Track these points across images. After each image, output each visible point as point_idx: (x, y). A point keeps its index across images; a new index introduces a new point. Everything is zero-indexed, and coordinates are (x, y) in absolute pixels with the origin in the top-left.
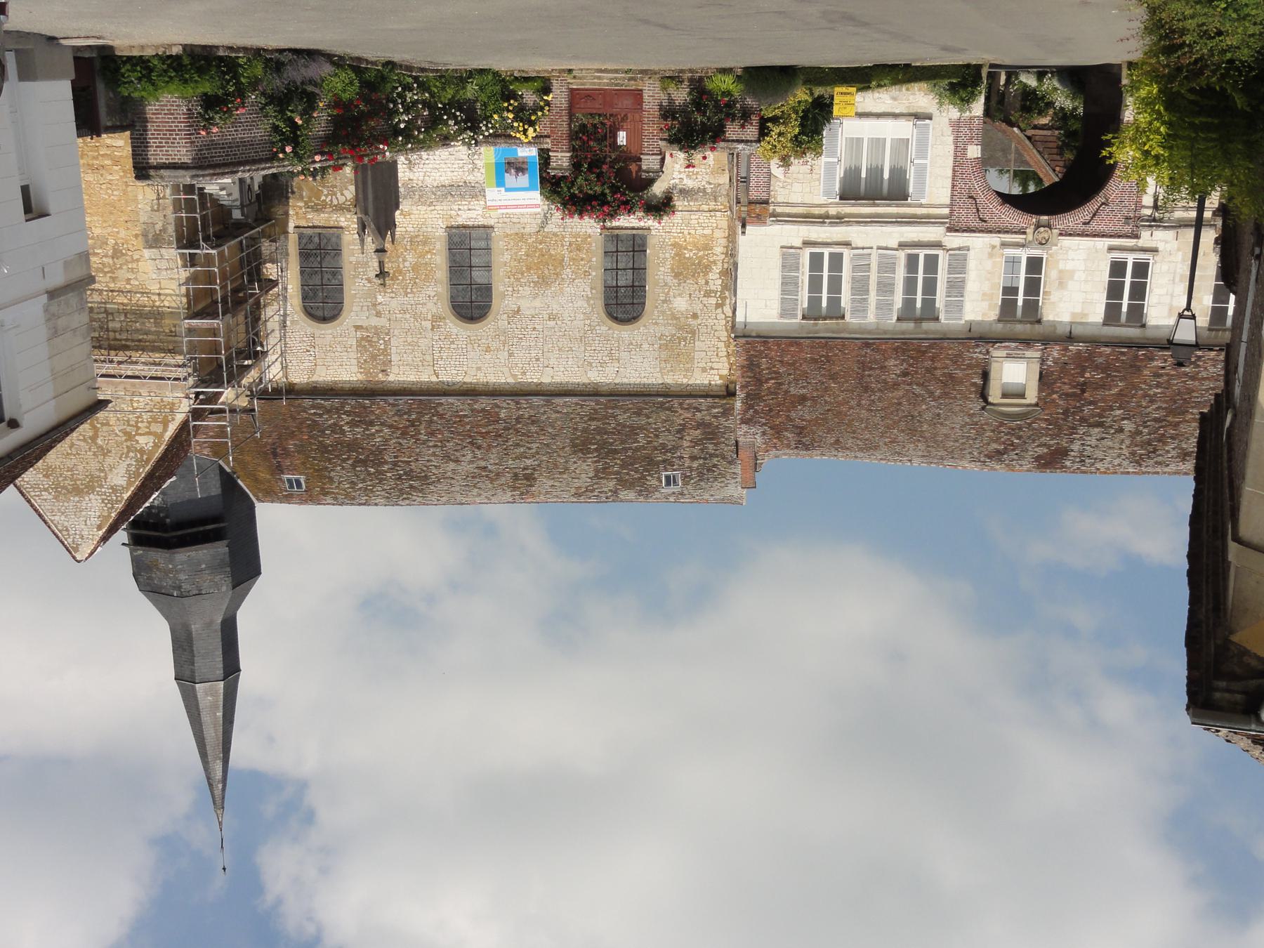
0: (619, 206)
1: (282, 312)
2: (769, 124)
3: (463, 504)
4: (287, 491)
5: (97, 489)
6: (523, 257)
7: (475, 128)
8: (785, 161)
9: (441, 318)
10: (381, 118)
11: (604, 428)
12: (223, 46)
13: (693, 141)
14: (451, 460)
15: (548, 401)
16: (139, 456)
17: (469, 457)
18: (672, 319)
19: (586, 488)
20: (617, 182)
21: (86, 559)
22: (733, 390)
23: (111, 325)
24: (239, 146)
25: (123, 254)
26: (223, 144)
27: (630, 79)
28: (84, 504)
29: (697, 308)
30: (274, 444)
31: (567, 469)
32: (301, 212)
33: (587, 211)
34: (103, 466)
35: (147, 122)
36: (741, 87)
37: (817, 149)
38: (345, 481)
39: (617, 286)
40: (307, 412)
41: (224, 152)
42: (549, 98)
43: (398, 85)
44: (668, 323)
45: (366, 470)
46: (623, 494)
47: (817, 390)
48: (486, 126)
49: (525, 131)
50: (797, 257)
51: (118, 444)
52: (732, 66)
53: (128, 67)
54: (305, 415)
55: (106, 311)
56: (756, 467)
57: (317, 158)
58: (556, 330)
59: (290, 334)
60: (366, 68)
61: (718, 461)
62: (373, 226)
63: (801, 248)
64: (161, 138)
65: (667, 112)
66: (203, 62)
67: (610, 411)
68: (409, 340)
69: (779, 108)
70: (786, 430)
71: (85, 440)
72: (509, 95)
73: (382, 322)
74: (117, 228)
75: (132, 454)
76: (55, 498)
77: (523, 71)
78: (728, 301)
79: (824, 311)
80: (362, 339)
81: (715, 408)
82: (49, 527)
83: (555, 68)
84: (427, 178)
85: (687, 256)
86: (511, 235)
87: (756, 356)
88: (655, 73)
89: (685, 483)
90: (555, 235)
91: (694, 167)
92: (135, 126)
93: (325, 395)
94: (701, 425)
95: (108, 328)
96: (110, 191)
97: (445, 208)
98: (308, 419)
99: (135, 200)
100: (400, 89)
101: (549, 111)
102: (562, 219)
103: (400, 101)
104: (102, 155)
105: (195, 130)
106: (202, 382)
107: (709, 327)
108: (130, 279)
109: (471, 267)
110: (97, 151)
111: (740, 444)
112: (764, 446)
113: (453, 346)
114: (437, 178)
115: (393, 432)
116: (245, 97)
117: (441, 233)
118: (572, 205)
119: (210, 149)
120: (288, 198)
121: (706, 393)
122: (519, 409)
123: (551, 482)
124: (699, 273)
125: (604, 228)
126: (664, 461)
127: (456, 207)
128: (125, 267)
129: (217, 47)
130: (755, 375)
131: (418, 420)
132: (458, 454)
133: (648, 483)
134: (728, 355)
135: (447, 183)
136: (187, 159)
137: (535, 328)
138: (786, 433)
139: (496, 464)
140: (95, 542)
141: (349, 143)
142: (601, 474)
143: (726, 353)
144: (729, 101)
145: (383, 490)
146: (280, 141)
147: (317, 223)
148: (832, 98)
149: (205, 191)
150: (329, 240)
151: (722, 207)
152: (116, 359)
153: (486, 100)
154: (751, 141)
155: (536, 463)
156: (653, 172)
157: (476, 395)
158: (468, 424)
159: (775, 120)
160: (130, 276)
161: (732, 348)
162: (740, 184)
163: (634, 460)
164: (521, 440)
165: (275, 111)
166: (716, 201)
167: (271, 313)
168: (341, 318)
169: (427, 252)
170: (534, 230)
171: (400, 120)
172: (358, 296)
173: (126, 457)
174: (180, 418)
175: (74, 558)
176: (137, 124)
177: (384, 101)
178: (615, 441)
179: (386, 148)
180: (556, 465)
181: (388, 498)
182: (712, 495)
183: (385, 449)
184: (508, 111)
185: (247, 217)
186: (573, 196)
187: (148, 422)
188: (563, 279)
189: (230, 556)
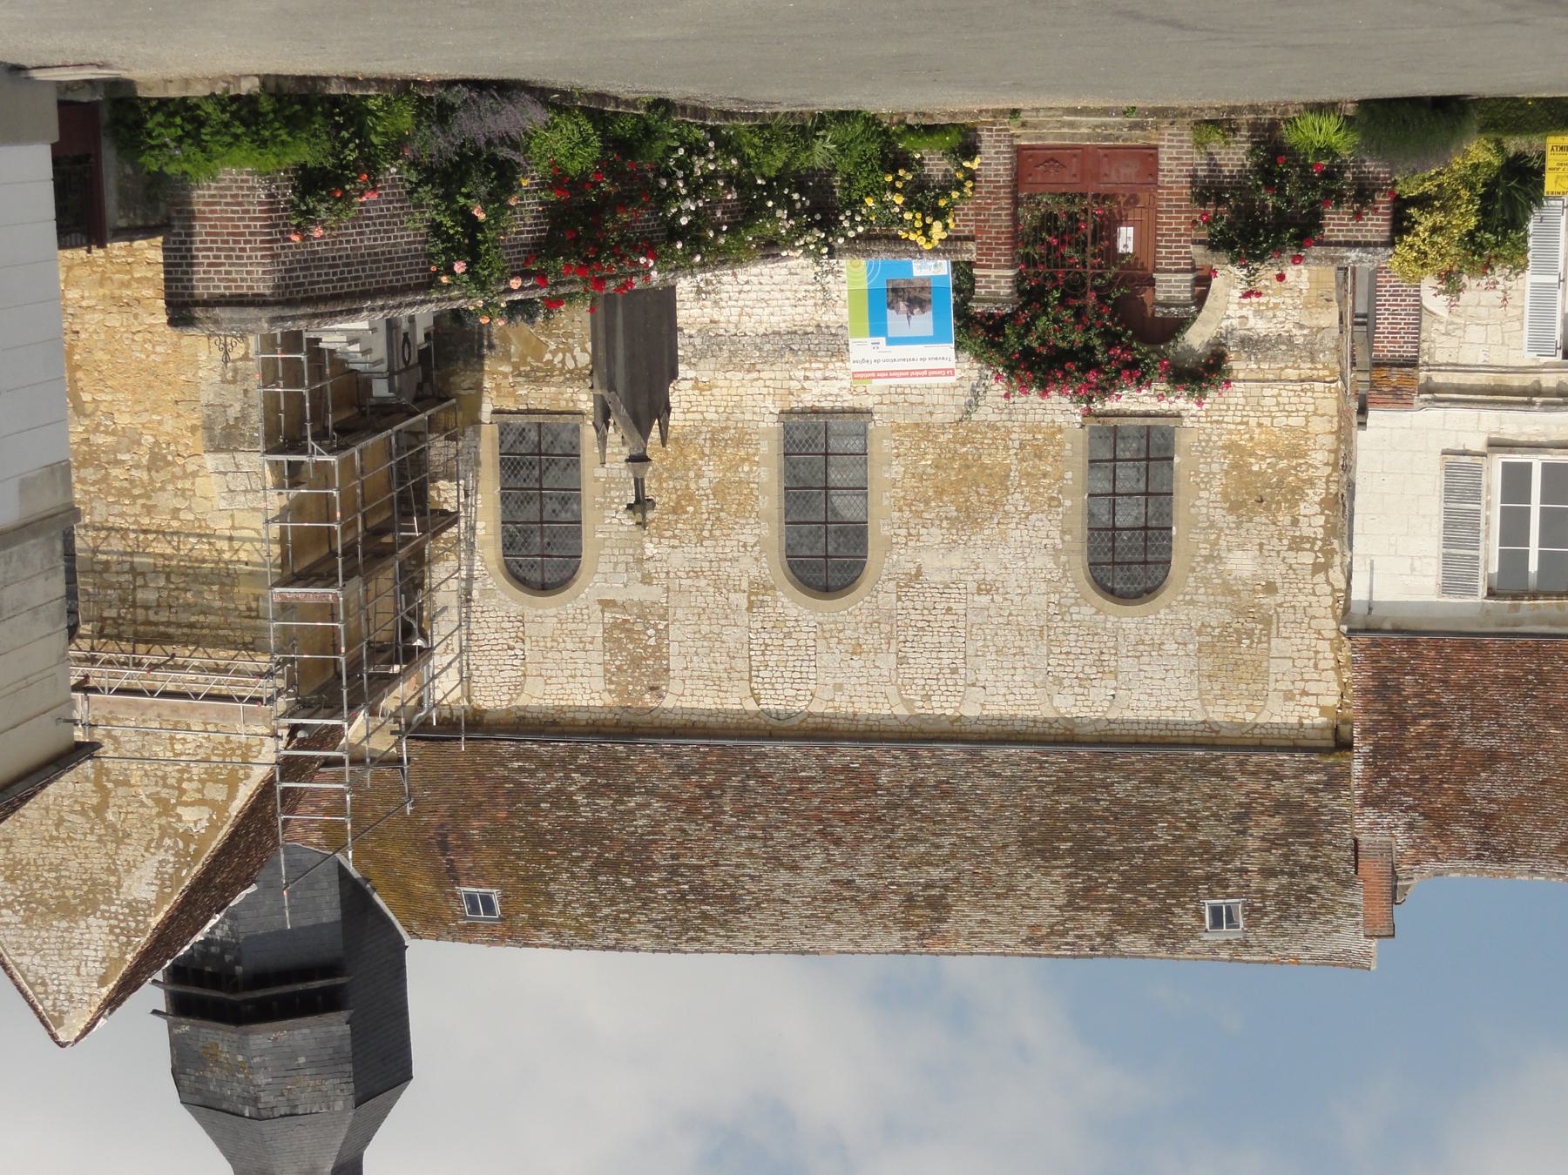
0: (1118, 372)
1: (463, 574)
2: (1413, 211)
3: (803, 953)
4: (465, 918)
5: (103, 907)
6: (929, 470)
7: (829, 224)
8: (1450, 282)
9: (767, 588)
10: (643, 206)
11: (1087, 810)
12: (338, 77)
13: (1257, 245)
14: (782, 865)
15: (973, 753)
16: (181, 844)
18: (1223, 594)
19: (1051, 926)
20: (1116, 325)
21: (77, 1040)
22: (1348, 737)
23: (141, 595)
24: (365, 263)
25: (169, 464)
26: (334, 258)
27: (1133, 126)
28: (76, 934)
29: (1276, 571)
30: (442, 826)
31: (1011, 889)
32: (505, 383)
33: (1055, 381)
34: (114, 863)
35: (194, 218)
36: (1354, 138)
37: (1516, 257)
39: (1114, 528)
40: (506, 767)
41: (335, 274)
42: (975, 165)
43: (676, 144)
44: (1216, 602)
45: (618, 881)
46: (1125, 942)
47: (1522, 740)
48: (852, 219)
49: (926, 229)
50: (1476, 472)
51: (145, 822)
52: (1336, 100)
53: (160, 117)
54: (501, 772)
55: (133, 570)
56: (1394, 895)
57: (515, 283)
58: (992, 612)
59: (478, 615)
60: (616, 114)
61: (1320, 880)
62: (623, 412)
63: (1483, 455)
64: (219, 249)
65: (1207, 190)
66: (297, 107)
67: (1098, 775)
68: (705, 629)
69: (1431, 178)
70: (1457, 820)
71: (83, 813)
72: (895, 160)
73: (654, 594)
74: (158, 414)
75: (168, 842)
76: (25, 921)
77: (924, 114)
78: (1337, 559)
79: (1533, 581)
80: (615, 625)
81: (1311, 772)
82: (12, 977)
83: (985, 107)
84: (745, 318)
85: (1255, 468)
86: (906, 428)
87: (1392, 671)
88: (1183, 115)
89: (1252, 924)
90: (993, 427)
91: (1259, 294)
92: (173, 227)
93: (541, 732)
94: (1282, 806)
95: (134, 601)
96: (148, 346)
97: (779, 375)
98: (506, 779)
99: (194, 363)
100: (681, 152)
101: (973, 189)
102: (1007, 396)
103: (680, 174)
104: (139, 280)
105: (281, 233)
106: (304, 706)
108: (180, 509)
109: (826, 488)
110: (129, 272)
111: (1363, 846)
112: (1411, 852)
113: (788, 642)
114: (765, 319)
116: (377, 170)
117: (770, 423)
118: (1026, 369)
119: (308, 268)
120: (481, 357)
121: (1293, 743)
122: (916, 768)
123: (980, 915)
124: (1279, 503)
125: (1088, 413)
126: (1208, 878)
127: (800, 374)
128: (170, 487)
129: (326, 79)
131: (719, 784)
132: (796, 854)
134: (1338, 667)
135: (783, 327)
136: (263, 288)
137: (950, 609)
138: (1456, 827)
139: (871, 875)
140: (94, 1009)
141: (579, 255)
142: (1081, 899)
143: (1332, 663)
144: (1330, 166)
145: (650, 921)
146: (444, 251)
147: (534, 404)
148: (1542, 156)
149: (321, 345)
150: (556, 436)
152: (146, 660)
153: (850, 169)
154: (1376, 245)
155: (950, 874)
156: (1177, 306)
157: (833, 739)
158: (815, 794)
159: (1423, 202)
160: (182, 504)
161: (1346, 652)
162: (1357, 328)
163: (1147, 874)
164: (921, 829)
165: (436, 196)
166: (1313, 361)
167: (443, 576)
168: (575, 587)
169: (743, 460)
170: (949, 418)
171: (679, 209)
173: (158, 847)
174: (259, 774)
175: (54, 1037)
176: (176, 223)
177: (651, 175)
178: (1109, 834)
179: (651, 263)
180: (989, 880)
181: (658, 936)
182: (1307, 949)
183: (655, 842)
184: (894, 190)
185: (399, 393)
186: (1028, 352)
187: (200, 780)
189: (353, 1041)
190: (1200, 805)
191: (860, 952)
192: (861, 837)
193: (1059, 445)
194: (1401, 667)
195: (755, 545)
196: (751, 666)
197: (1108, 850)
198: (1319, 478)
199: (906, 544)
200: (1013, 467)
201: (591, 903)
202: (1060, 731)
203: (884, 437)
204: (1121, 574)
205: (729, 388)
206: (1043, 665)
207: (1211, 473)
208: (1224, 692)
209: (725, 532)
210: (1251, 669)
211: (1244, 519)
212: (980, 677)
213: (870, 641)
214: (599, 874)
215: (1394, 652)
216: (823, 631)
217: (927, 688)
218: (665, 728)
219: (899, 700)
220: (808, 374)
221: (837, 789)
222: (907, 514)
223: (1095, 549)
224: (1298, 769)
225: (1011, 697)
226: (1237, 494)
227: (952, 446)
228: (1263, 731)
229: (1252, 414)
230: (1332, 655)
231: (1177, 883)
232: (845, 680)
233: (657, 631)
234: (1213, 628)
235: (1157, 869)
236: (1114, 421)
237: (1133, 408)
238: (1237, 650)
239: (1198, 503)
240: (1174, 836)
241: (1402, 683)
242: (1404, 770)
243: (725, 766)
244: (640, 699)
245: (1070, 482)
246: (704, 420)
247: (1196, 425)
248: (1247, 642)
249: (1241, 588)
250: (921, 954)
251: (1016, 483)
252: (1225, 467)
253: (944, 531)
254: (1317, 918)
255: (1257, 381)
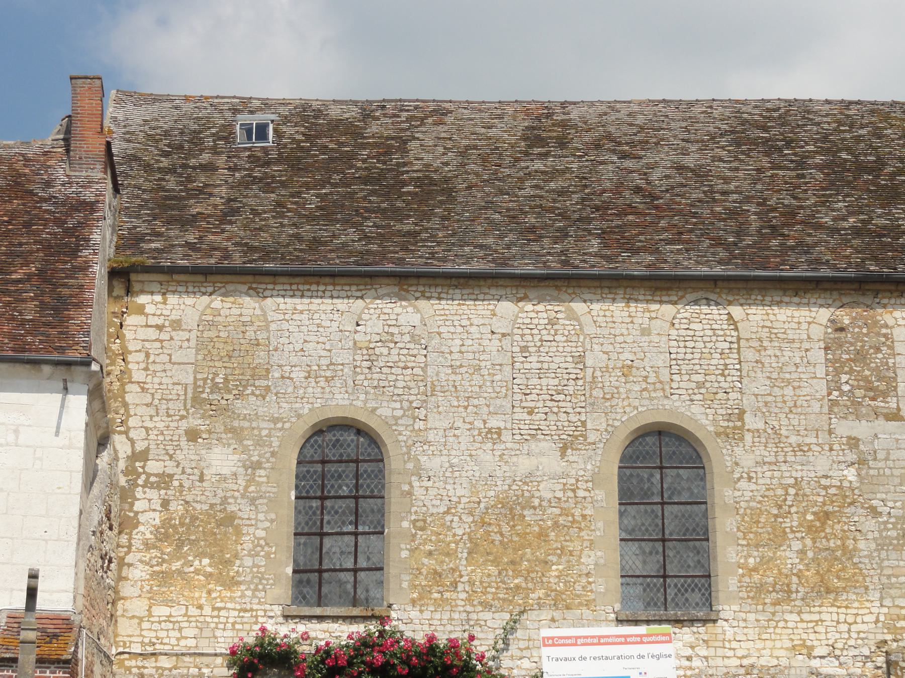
0: (350, 664)
6: (554, 559)
9: (723, 434)
14: (692, 171)
17: (655, 176)
18: (242, 429)
19: (423, 124)
22: (115, 283)
29: (187, 453)
33: (419, 655)
38: (893, 140)
44: (250, 421)
45: (856, 157)
46: (353, 113)
61: (158, 161)
67: (374, 247)
68: (789, 391)
73: (845, 428)
78: (122, 465)
80: (885, 394)
85: (206, 561)
86: (580, 604)
87: (46, 324)
90: (486, 606)
97: (719, 662)
102: (472, 638)
107: (162, 412)
113: (700, 378)
115: (814, 217)
117: (727, 609)
118: (452, 666)
123: (492, 132)
124: (182, 524)
125: (383, 620)
126: (268, 164)
127: (696, 663)
130: (53, 290)
132: (679, 179)
133: (302, 129)
134: (124, 355)
137: (530, 413)
139: (602, 163)
143: (130, 358)
145: (818, 124)
151: (127, 663)
155: (523, 164)
158: (665, 230)
164: (554, 201)
169: (755, 569)
170: (533, 615)
172: (897, 481)
178: (364, 198)
180: (484, 160)
181: (809, 112)
182: (176, 108)
183: (823, 189)
188: (471, 514)
190: (271, 222)
191: (609, 102)
192: (614, 194)
193: (415, 587)
194: (35, 327)
195: (739, 479)
196: (739, 353)
197: (366, 185)
198: (139, 551)
199: (577, 481)
200: (464, 562)
201: (879, 138)
202: (414, 288)
203: (604, 594)
204: (349, 450)
205: (773, 648)
206: (432, 357)
207: (252, 556)
208: (243, 329)
209: (771, 493)
210: (215, 352)
211: (218, 508)
212: (497, 343)
213: (612, 380)
214: (875, 162)
215: (41, 342)
216: (663, 390)
217: (552, 332)
218: (825, 290)
219: (582, 319)
220: (687, 663)
221: (642, 234)
222: (577, 512)
223: (376, 476)
224: (170, 252)
225: (464, 323)
226: (225, 534)
227: (530, 585)
228: (203, 289)
229: (208, 619)
230: (130, 366)
231: (299, 159)
232: (638, 339)
233: (839, 389)
234: (253, 394)
235: (318, 169)
236: (356, 612)
237: (336, 626)
238: (229, 371)
239: (268, 524)
240: (299, 197)
241: (36, 312)
242: (48, 233)
243: (760, 254)
244: (854, 319)
245: (403, 546)
246: (799, 613)
247: (268, 607)
248: (218, 380)
249: (223, 436)
250: (549, 102)
251: (461, 545)
252: (238, 562)
253: (537, 494)
254: (166, 131)
255: (202, 654)
